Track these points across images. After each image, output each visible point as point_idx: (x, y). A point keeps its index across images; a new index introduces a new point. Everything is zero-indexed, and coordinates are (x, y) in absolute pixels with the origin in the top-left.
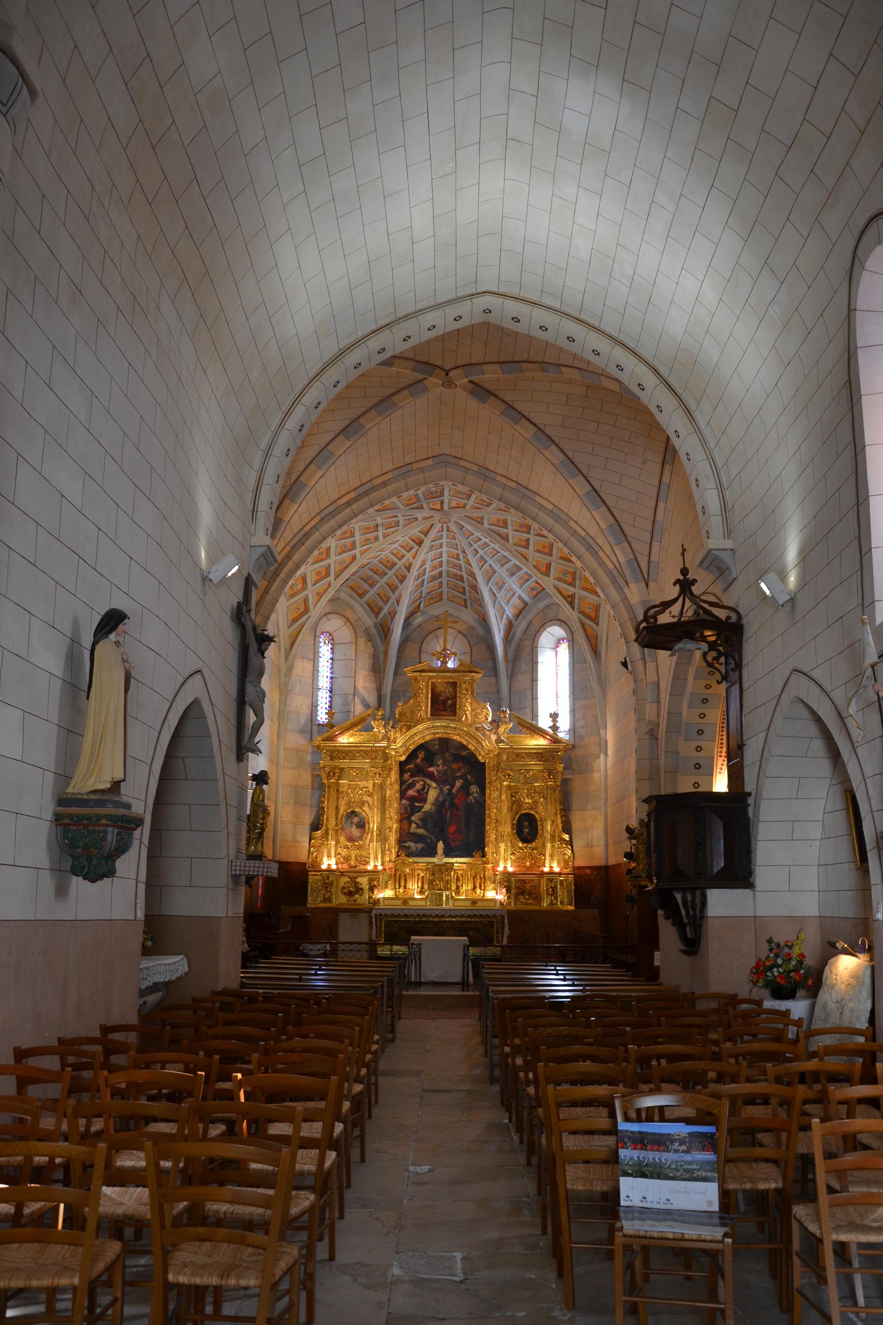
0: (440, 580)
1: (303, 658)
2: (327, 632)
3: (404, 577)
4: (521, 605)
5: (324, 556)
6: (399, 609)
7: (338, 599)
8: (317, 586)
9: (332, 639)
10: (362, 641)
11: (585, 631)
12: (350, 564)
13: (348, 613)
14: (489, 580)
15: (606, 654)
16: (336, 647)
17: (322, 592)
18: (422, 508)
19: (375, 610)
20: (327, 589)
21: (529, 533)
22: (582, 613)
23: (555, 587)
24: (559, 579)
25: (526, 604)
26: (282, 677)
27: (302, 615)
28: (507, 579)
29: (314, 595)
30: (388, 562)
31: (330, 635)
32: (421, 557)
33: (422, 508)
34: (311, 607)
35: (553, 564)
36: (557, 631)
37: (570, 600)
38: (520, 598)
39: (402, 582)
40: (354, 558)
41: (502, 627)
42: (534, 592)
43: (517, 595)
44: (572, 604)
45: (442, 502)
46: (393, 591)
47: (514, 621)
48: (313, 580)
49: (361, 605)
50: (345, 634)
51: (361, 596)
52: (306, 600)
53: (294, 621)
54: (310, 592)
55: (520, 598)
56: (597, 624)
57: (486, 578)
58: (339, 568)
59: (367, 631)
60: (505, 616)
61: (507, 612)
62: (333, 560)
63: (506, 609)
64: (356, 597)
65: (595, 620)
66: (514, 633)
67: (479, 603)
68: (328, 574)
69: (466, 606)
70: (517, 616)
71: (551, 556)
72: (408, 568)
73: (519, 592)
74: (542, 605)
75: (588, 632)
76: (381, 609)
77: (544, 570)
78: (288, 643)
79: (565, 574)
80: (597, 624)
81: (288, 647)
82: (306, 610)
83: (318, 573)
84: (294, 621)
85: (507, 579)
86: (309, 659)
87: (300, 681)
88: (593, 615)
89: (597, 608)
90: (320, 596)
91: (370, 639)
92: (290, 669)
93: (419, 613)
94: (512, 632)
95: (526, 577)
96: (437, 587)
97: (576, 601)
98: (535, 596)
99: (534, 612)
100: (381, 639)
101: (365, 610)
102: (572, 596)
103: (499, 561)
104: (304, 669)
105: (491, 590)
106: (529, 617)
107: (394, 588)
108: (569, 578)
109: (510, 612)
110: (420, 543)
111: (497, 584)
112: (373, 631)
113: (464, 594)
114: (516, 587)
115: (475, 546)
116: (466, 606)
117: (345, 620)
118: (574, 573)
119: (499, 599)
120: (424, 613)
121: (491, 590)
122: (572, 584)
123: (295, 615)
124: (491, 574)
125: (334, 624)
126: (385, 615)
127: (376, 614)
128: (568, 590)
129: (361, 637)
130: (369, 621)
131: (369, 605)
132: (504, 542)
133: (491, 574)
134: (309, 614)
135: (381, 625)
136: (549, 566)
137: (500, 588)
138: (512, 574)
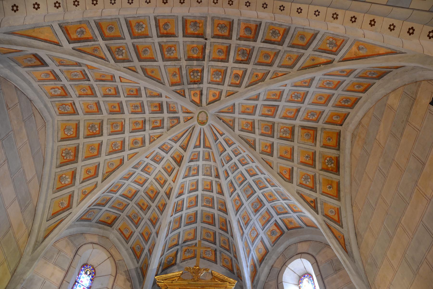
0: (194, 226)
1: (55, 264)
2: (91, 266)
3: (165, 205)
4: (263, 251)
5: (96, 153)
6: (157, 240)
7: (107, 238)
8: (84, 184)
9: (95, 273)
10: (121, 278)
11: (332, 232)
12: (118, 167)
13: (113, 252)
14: (237, 210)
15: (359, 248)
16: (96, 279)
17: (87, 192)
18: (184, 96)
19: (136, 253)
20: (93, 190)
21: (273, 137)
22: (326, 216)
23: (298, 193)
24: (301, 185)
25: (267, 252)
26: (21, 266)
27: (64, 210)
28: (252, 215)
29: (80, 193)
30: (152, 191)
31: (94, 269)
32: (180, 180)
33: (184, 96)
34: (75, 204)
35: (295, 169)
36: (301, 264)
37: (313, 205)
38: (262, 241)
39: (162, 212)
40: (122, 161)
41: (249, 264)
42: (274, 237)
43: (259, 237)
44: (315, 208)
45: (201, 94)
46: (154, 225)
47: (258, 266)
48: (82, 178)
49: (127, 250)
50: (106, 267)
51: (127, 239)
52: (71, 196)
53: (55, 215)
54: (77, 189)
55: (262, 241)
56: (342, 226)
57: (235, 208)
58: (107, 170)
59: (128, 272)
60: (250, 256)
61: (252, 252)
62: (102, 159)
63: (252, 249)
64: (122, 239)
65: (339, 222)
66: (259, 278)
67: (230, 247)
68: (96, 175)
69: (215, 262)
70: (261, 261)
71: (293, 161)
72: (168, 195)
73: (262, 234)
74: (281, 249)
75: (335, 233)
76: (142, 250)
77: (287, 176)
78: (42, 235)
79: (306, 179)
80: (342, 226)
81: (41, 239)
82: (69, 206)
83: (88, 171)
84: (55, 215)
85: (252, 215)
86: (62, 268)
87: (44, 283)
88: (336, 218)
89: (338, 211)
90: (85, 195)
91: (129, 279)
92: (33, 260)
93: (175, 267)
94: (256, 278)
95: (267, 217)
96: (191, 237)
97: (319, 205)
98: (274, 242)
99: (274, 257)
100: (140, 285)
101: (130, 255)
102: (315, 202)
103: (245, 191)
104: (52, 274)
105: (239, 222)
106: (271, 262)
107: (154, 221)
108: (309, 183)
109: (255, 255)
110: (179, 161)
111: (244, 218)
112: (134, 274)
113: (215, 243)
114: (258, 227)
115: (227, 166)
116: (215, 262)
117: (109, 255)
118: (314, 177)
119: (245, 235)
120: (180, 268)
121: (239, 222)
122: (313, 189)
123: (58, 209)
124: (239, 207)
125: (95, 255)
126: (146, 255)
127: (138, 257)
128: (310, 195)
129: (121, 274)
130: (131, 264)
131: (133, 249)
132: (252, 150)
133: (239, 207)
134: (70, 211)
135: (141, 269)
136: (291, 171)
137: (247, 224)
138: (256, 211)
